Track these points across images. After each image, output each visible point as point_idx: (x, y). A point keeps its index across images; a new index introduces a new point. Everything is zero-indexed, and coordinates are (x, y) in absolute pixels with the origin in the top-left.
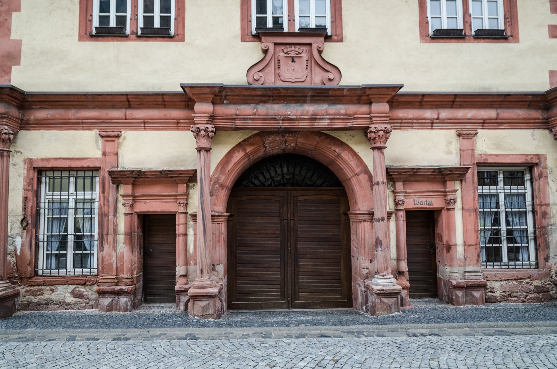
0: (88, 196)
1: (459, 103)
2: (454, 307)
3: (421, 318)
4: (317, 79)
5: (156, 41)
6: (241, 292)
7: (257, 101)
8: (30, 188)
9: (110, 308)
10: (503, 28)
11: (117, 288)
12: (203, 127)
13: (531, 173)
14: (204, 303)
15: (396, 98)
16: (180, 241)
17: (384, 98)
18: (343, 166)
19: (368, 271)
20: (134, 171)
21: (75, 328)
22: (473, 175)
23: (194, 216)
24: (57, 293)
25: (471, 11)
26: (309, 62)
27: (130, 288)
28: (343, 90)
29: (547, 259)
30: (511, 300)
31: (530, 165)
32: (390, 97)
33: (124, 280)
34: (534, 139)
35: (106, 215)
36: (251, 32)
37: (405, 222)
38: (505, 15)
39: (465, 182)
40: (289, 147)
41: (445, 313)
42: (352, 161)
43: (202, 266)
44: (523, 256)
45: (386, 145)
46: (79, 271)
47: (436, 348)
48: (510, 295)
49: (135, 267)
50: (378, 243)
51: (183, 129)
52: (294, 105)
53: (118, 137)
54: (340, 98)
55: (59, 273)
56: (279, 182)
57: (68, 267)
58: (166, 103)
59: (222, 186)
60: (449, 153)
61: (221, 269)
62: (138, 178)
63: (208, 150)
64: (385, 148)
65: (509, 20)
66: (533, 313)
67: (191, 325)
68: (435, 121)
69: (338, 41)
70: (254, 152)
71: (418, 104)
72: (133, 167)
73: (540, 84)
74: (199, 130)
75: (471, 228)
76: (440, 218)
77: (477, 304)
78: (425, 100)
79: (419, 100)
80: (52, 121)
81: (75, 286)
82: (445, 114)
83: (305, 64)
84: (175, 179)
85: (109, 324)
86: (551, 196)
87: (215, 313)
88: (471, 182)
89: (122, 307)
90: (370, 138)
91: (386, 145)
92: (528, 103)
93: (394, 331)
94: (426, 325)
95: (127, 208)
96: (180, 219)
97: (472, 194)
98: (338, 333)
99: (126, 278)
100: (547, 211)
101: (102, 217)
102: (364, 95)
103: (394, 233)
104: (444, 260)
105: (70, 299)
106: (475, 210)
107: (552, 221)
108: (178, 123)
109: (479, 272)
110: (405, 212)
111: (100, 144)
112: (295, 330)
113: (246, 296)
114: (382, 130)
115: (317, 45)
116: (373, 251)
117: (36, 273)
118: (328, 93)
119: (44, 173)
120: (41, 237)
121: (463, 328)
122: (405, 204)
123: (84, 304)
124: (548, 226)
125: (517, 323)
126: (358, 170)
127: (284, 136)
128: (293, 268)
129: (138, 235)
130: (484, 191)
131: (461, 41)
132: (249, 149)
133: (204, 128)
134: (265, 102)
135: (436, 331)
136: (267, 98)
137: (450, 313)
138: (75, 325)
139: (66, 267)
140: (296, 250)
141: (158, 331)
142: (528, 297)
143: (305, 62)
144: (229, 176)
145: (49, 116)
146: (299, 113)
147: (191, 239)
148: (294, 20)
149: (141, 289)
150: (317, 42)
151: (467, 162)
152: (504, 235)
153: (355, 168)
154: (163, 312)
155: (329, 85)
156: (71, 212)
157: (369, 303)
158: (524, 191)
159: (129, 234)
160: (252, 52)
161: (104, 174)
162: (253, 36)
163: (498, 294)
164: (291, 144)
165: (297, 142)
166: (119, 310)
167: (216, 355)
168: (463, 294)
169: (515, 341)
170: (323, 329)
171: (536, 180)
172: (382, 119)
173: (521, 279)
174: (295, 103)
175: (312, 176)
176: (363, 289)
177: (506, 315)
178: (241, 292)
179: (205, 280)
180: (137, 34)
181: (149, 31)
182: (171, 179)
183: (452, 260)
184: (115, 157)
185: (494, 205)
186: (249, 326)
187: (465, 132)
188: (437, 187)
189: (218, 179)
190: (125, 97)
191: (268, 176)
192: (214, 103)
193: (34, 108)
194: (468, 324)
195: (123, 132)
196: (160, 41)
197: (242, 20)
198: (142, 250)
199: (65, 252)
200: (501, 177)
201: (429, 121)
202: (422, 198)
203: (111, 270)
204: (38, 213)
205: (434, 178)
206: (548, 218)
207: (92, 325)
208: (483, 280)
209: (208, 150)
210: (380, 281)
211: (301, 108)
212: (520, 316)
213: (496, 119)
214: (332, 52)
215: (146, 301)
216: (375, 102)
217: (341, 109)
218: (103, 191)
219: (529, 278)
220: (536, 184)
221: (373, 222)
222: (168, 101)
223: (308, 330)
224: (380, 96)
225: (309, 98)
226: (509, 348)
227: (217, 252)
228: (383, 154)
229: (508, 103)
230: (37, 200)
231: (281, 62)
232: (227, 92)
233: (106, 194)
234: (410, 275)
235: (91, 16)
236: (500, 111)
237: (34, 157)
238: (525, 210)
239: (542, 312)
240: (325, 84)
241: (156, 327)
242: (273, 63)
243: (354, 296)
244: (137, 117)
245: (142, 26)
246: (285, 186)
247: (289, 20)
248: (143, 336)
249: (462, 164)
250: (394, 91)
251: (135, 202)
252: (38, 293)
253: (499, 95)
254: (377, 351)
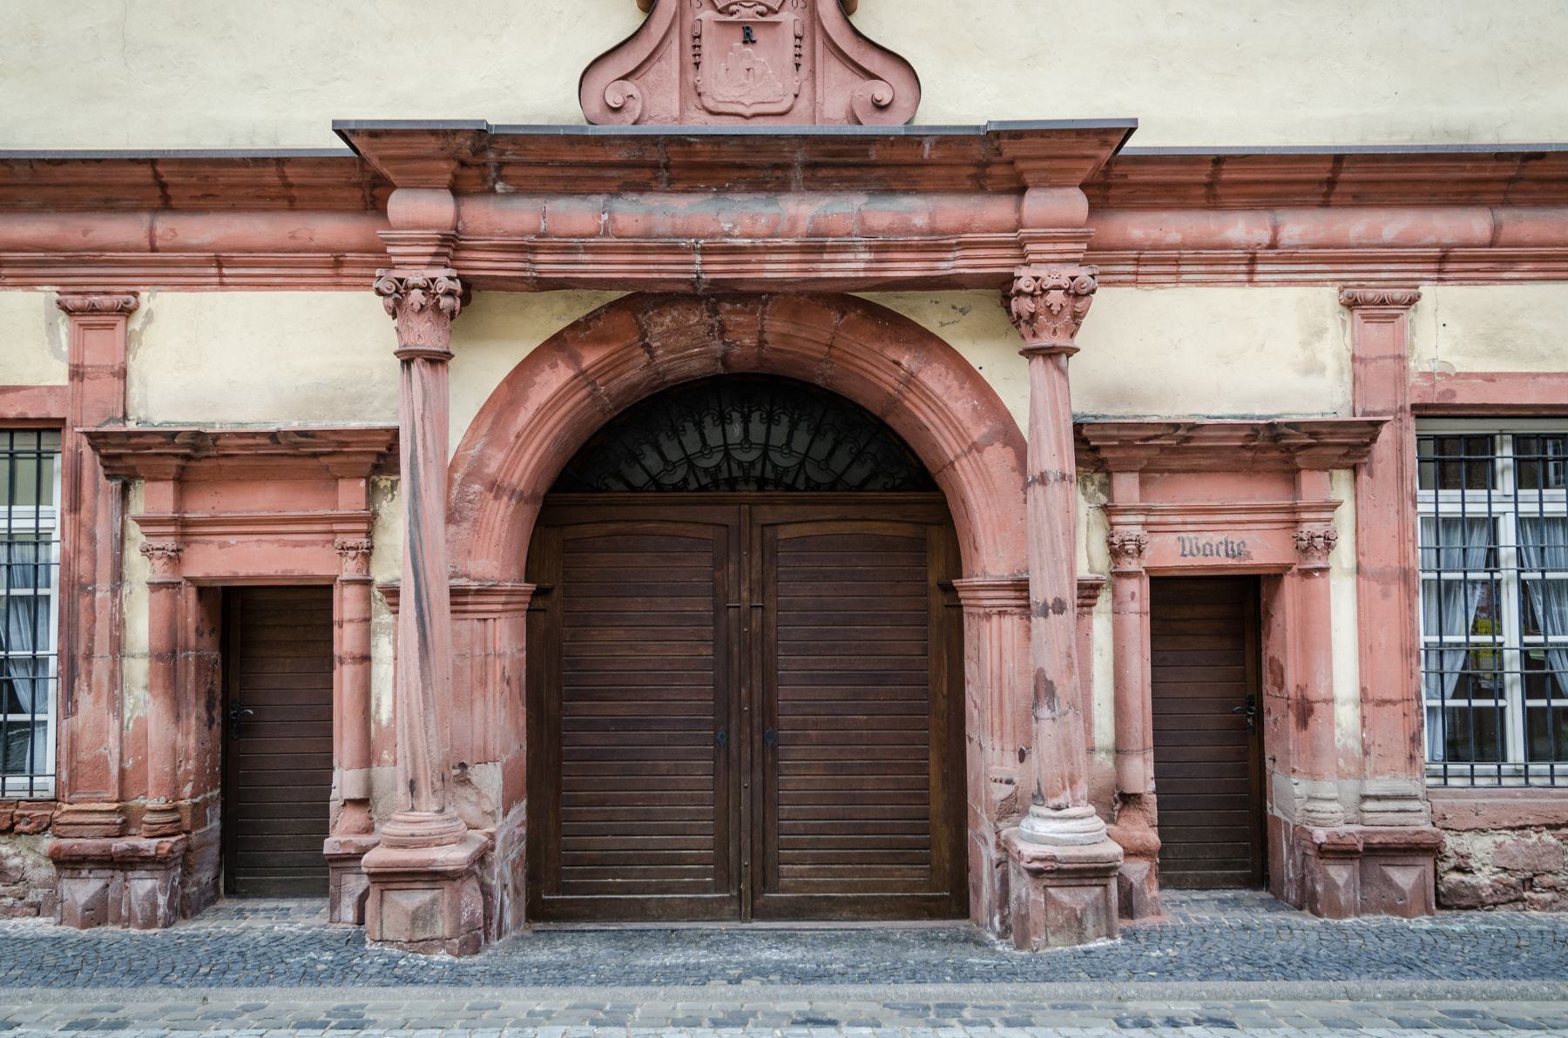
1: (1353, 189)
2: (1317, 921)
3: (1186, 962)
4: (834, 105)
6: (576, 861)
7: (613, 186)
9: (98, 913)
11: (120, 845)
12: (416, 276)
15: (1118, 170)
16: (344, 678)
17: (1073, 170)
18: (926, 416)
19: (1009, 789)
22: (1400, 450)
23: (392, 593)
26: (806, 44)
27: (168, 843)
28: (920, 143)
30: (1532, 902)
32: (1089, 166)
35: (83, 587)
37: (1147, 619)
40: (737, 351)
41: (1275, 946)
42: (957, 399)
43: (415, 768)
45: (1077, 341)
48: (1528, 883)
49: (187, 772)
50: (1043, 689)
51: (356, 286)
52: (746, 197)
53: (126, 311)
54: (911, 172)
56: (714, 472)
58: (295, 192)
59: (495, 487)
60: (1312, 368)
61: (490, 779)
62: (194, 458)
63: (438, 360)
64: (1071, 351)
68: (1261, 253)
70: (612, 366)
71: (1203, 191)
72: (180, 419)
74: (403, 287)
75: (1388, 637)
76: (1277, 604)
77: (1403, 912)
79: (1204, 178)
82: (1298, 227)
83: (791, 51)
84: (324, 460)
85: (76, 972)
87: (456, 932)
88: (1392, 473)
89: (137, 909)
90: (1019, 316)
91: (1077, 341)
93: (1073, 1007)
95: (159, 563)
96: (346, 604)
97: (1393, 517)
99: (154, 811)
101: (71, 596)
102: (996, 159)
103: (1110, 658)
104: (1288, 752)
106: (1406, 576)
108: (338, 263)
110: (1146, 582)
111: (64, 339)
113: (592, 874)
114: (1059, 288)
116: (1028, 717)
118: (866, 153)
121: (1329, 999)
122: (1147, 553)
125: (1532, 985)
126: (978, 432)
127: (715, 312)
128: (758, 777)
129: (198, 658)
130: (1443, 508)
133: (420, 281)
134: (642, 188)
135: (1226, 1009)
136: (648, 173)
137: (1294, 944)
140: (769, 712)
141: (239, 997)
143: (791, 41)
147: (383, 672)
149: (214, 850)
151: (1380, 403)
153: (968, 423)
154: (281, 928)
155: (873, 125)
157: (1013, 905)
159: (167, 657)
161: (78, 445)
163: (1483, 879)
164: (746, 337)
165: (762, 332)
166: (128, 921)
168: (1352, 877)
170: (820, 998)
175: (831, 453)
177: (1502, 953)
178: (576, 861)
182: (312, 462)
183: (1314, 753)
184: (117, 384)
185: (1478, 554)
186: (566, 981)
187: (1370, 294)
188: (1267, 493)
189: (480, 461)
191: (674, 454)
192: (457, 191)
194: (1352, 984)
198: (217, 713)
200: (1505, 457)
202: (1212, 531)
203: (100, 782)
205: (1254, 461)
207: (17, 972)
208: (1428, 827)
209: (438, 360)
210: (1045, 828)
213: (1491, 245)
215: (232, 891)
216: (1037, 186)
217: (915, 211)
218: (74, 503)
221: (1029, 619)
223: (769, 998)
225: (798, 174)
228: (1063, 372)
229: (1536, 187)
231: (706, 42)
232: (502, 152)
233: (84, 514)
234: (1161, 805)
236: (1504, 215)
240: (859, 123)
241: (236, 983)
242: (675, 46)
243: (971, 879)
244: (194, 241)
246: (733, 489)
248: (176, 1015)
249: (1359, 410)
251: (188, 544)
253: (1501, 157)
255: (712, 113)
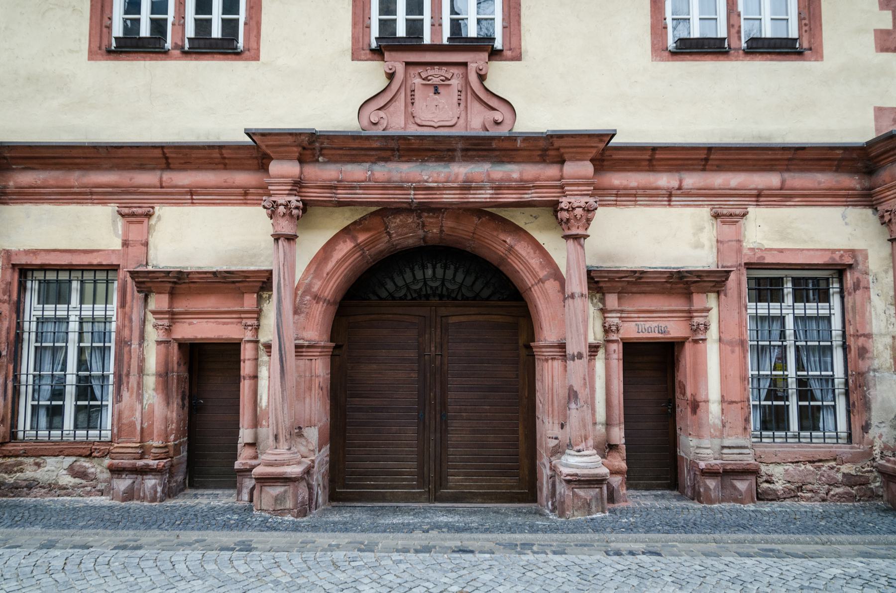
0: (99, 313)
3: (639, 524)
4: (476, 121)
5: (213, 59)
6: (352, 473)
7: (373, 159)
8: (6, 297)
9: (129, 495)
10: (796, 36)
11: (140, 463)
12: (281, 200)
13: (841, 282)
14: (277, 490)
15: (608, 153)
16: (245, 386)
18: (518, 266)
19: (556, 442)
20: (170, 272)
21: (62, 527)
23: (268, 347)
24: (46, 469)
25: (741, 8)
26: (463, 94)
28: (516, 140)
29: (866, 428)
30: (802, 497)
31: (839, 267)
32: (594, 151)
33: (153, 450)
34: (846, 224)
35: (126, 343)
36: (370, 45)
37: (621, 362)
38: (799, 14)
39: (726, 295)
40: (430, 235)
42: (533, 258)
44: (826, 419)
45: (589, 232)
46: (81, 433)
47: (646, 576)
48: (800, 489)
49: (172, 429)
50: (572, 395)
52: (435, 164)
53: (149, 215)
55: (49, 437)
57: (66, 427)
58: (227, 161)
59: (317, 298)
60: (698, 246)
61: (313, 434)
62: (178, 283)
63: (291, 238)
65: (807, 22)
66: (835, 520)
67: (251, 526)
68: (674, 192)
69: (513, 59)
71: (647, 163)
73: (857, 128)
77: (741, 502)
78: (657, 156)
79: (647, 157)
80: (42, 190)
81: (74, 459)
82: (692, 180)
83: (456, 98)
84: (237, 284)
85: (118, 522)
86: (874, 321)
87: (295, 507)
89: (148, 493)
90: (562, 220)
91: (589, 232)
92: (836, 163)
93: (585, 546)
94: (643, 536)
95: (161, 332)
96: (247, 352)
97: (736, 315)
98: (489, 545)
99: (156, 447)
100: (867, 346)
102: (551, 148)
104: (687, 425)
105: (67, 480)
107: (876, 363)
109: (746, 448)
110: (621, 345)
112: (420, 539)
113: (360, 480)
115: (475, 65)
117: (13, 436)
118: (490, 144)
119: (29, 274)
120: (23, 378)
121: (706, 543)
122: (621, 331)
123: (89, 488)
124: (868, 372)
125: (802, 537)
126: (542, 274)
128: (438, 435)
129: (178, 376)
130: (46, 313)
131: (721, 57)
132: (362, 238)
134: (386, 160)
135: (657, 547)
136: (389, 153)
137: (690, 517)
138: (63, 523)
139: (61, 428)
140: (444, 404)
141: (194, 535)
142: (832, 493)
143: (456, 93)
144: (328, 281)
145: (39, 182)
146: (443, 178)
147: (263, 383)
148: (440, 25)
149: (184, 466)
150: (476, 60)
151: (730, 262)
152: (792, 385)
153: (537, 269)
155: (494, 132)
156: (73, 337)
157: (558, 496)
158: (827, 312)
159: (164, 375)
160: (370, 77)
161: (125, 277)
162: (372, 50)
163: (779, 486)
164: (434, 229)
165: (442, 226)
166: (143, 499)
167: (267, 579)
169: (788, 568)
171: (850, 294)
172: (580, 188)
173: (820, 461)
174: (436, 161)
176: (549, 473)
177: (787, 522)
178: (352, 473)
179: (282, 452)
180: (183, 47)
181: (202, 42)
182: (232, 286)
183: (700, 426)
184: (144, 248)
185: (776, 333)
186: (346, 530)
187: (725, 211)
188: (677, 304)
189: (310, 285)
190: (159, 151)
191: (400, 283)
192: (301, 161)
193: (14, 169)
194: (717, 536)
195: (157, 208)
196: (220, 60)
197: (355, 24)
199: (61, 403)
200: (788, 288)
201: (664, 192)
202: (652, 322)
203: (132, 433)
204: (19, 339)
205: (671, 288)
206: (868, 358)
208: (753, 462)
211: (447, 170)
212: (809, 526)
213: (781, 189)
214: (502, 77)
215: (192, 486)
216: (570, 160)
217: (514, 171)
218: (123, 304)
219: (835, 460)
220: (849, 300)
222: (230, 158)
223: (442, 540)
224: (579, 150)
225: (459, 154)
226: (772, 580)
227: (307, 406)
228: (582, 246)
229: (802, 163)
230: (18, 317)
232: (322, 143)
233: (127, 308)
235: (110, 19)
236: (787, 175)
237: (13, 248)
238: (829, 343)
239: (851, 519)
241: (192, 529)
243: (538, 484)
244: (180, 183)
245: (192, 35)
246: (428, 300)
247: (433, 25)
248: (164, 544)
249: (720, 265)
250: (601, 141)
251: (174, 323)
252: (15, 469)
253: (785, 149)
254: (542, 578)
255: (419, 125)
